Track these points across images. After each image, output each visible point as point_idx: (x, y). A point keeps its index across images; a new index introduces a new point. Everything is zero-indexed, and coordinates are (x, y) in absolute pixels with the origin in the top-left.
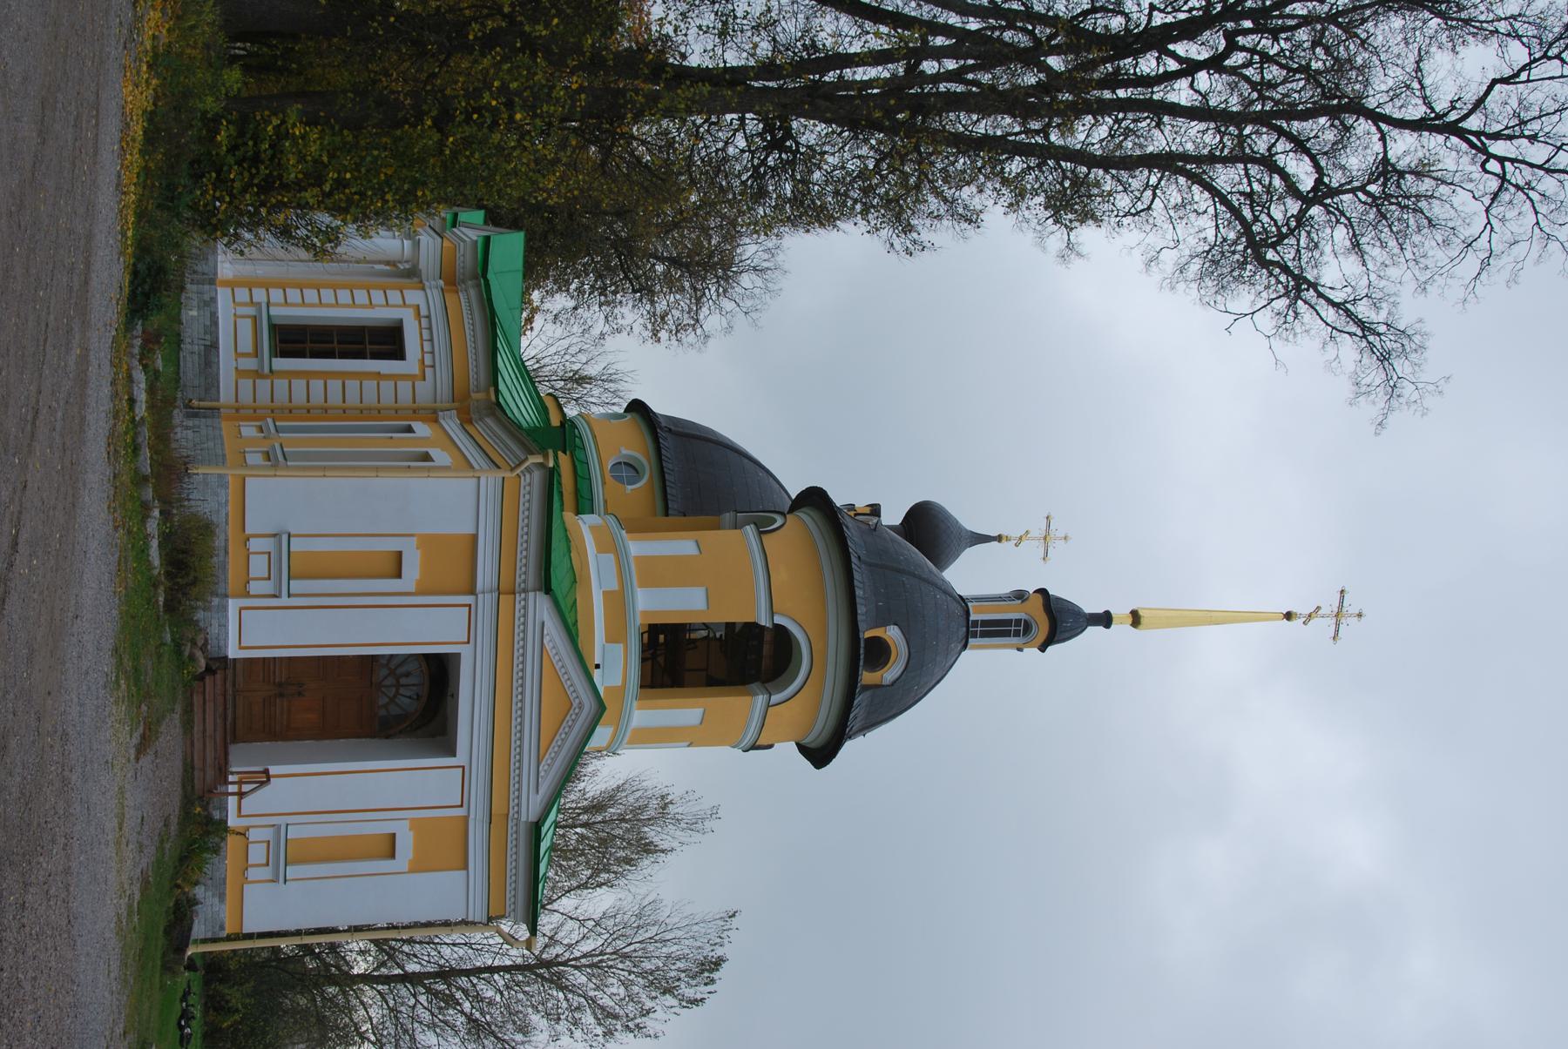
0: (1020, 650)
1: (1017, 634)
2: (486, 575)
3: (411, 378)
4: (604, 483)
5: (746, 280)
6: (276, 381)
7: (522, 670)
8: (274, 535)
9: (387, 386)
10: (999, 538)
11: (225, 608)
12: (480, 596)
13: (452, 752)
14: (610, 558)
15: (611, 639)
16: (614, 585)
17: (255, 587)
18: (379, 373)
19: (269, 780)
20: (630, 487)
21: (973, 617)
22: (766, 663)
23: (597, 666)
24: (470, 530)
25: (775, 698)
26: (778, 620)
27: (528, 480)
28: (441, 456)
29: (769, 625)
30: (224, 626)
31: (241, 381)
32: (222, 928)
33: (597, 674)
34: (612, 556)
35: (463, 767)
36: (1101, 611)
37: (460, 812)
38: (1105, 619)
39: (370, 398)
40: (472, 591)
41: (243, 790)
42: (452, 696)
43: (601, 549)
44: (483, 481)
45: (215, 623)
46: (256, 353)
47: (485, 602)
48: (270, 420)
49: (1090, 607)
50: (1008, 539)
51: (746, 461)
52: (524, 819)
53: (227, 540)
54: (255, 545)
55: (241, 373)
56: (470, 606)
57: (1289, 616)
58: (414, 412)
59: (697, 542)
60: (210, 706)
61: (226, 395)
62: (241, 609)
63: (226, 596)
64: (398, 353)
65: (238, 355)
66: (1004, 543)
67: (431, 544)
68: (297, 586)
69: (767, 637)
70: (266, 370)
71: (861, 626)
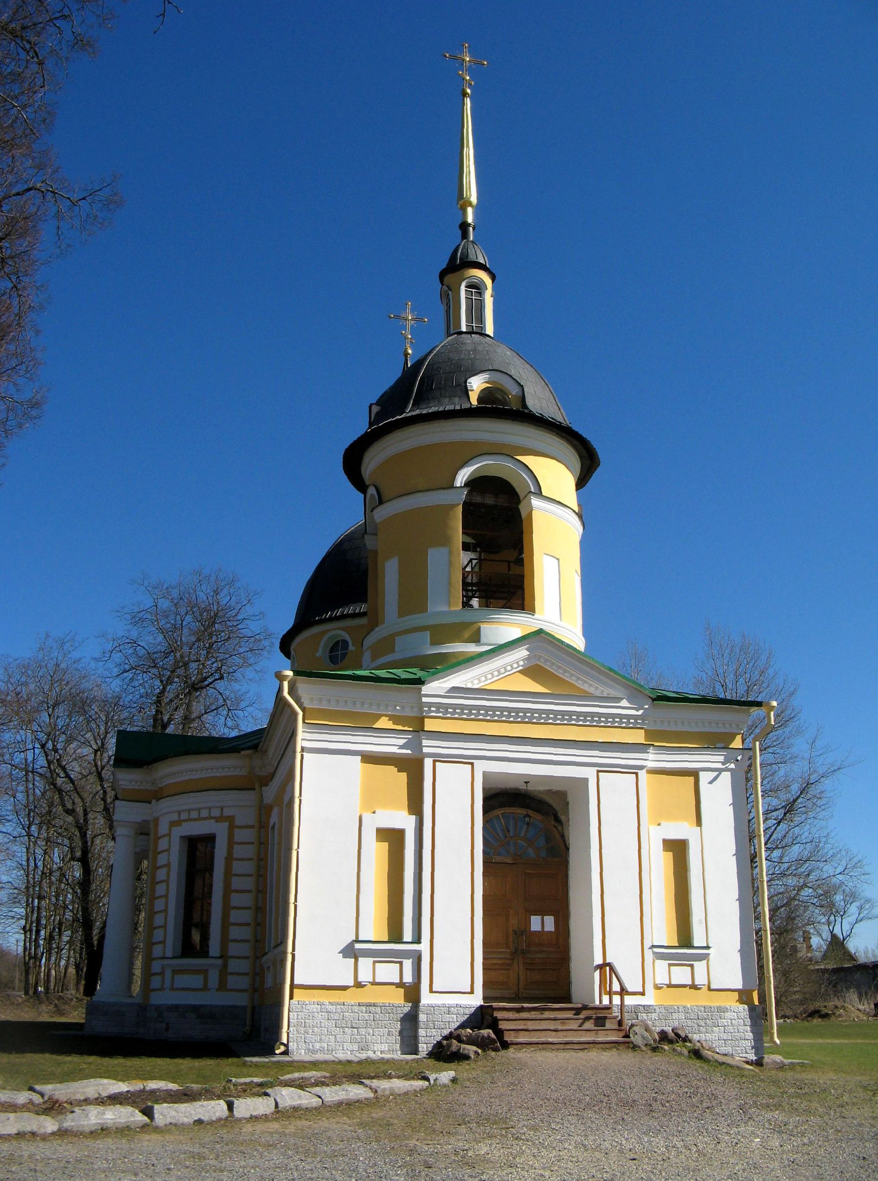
3: (232, 827)
5: (223, 598)
9: (238, 851)
19: (609, 965)
30: (449, 1009)
31: (229, 986)
34: (608, 996)
41: (619, 990)
42: (526, 783)
44: (307, 744)
45: (447, 1017)
46: (204, 972)
55: (222, 986)
56: (434, 761)
61: (242, 1000)
62: (431, 991)
64: (210, 839)
65: (205, 988)
67: (371, 801)
68: (408, 935)
69: (478, 499)
70: (219, 962)
71: (466, 406)
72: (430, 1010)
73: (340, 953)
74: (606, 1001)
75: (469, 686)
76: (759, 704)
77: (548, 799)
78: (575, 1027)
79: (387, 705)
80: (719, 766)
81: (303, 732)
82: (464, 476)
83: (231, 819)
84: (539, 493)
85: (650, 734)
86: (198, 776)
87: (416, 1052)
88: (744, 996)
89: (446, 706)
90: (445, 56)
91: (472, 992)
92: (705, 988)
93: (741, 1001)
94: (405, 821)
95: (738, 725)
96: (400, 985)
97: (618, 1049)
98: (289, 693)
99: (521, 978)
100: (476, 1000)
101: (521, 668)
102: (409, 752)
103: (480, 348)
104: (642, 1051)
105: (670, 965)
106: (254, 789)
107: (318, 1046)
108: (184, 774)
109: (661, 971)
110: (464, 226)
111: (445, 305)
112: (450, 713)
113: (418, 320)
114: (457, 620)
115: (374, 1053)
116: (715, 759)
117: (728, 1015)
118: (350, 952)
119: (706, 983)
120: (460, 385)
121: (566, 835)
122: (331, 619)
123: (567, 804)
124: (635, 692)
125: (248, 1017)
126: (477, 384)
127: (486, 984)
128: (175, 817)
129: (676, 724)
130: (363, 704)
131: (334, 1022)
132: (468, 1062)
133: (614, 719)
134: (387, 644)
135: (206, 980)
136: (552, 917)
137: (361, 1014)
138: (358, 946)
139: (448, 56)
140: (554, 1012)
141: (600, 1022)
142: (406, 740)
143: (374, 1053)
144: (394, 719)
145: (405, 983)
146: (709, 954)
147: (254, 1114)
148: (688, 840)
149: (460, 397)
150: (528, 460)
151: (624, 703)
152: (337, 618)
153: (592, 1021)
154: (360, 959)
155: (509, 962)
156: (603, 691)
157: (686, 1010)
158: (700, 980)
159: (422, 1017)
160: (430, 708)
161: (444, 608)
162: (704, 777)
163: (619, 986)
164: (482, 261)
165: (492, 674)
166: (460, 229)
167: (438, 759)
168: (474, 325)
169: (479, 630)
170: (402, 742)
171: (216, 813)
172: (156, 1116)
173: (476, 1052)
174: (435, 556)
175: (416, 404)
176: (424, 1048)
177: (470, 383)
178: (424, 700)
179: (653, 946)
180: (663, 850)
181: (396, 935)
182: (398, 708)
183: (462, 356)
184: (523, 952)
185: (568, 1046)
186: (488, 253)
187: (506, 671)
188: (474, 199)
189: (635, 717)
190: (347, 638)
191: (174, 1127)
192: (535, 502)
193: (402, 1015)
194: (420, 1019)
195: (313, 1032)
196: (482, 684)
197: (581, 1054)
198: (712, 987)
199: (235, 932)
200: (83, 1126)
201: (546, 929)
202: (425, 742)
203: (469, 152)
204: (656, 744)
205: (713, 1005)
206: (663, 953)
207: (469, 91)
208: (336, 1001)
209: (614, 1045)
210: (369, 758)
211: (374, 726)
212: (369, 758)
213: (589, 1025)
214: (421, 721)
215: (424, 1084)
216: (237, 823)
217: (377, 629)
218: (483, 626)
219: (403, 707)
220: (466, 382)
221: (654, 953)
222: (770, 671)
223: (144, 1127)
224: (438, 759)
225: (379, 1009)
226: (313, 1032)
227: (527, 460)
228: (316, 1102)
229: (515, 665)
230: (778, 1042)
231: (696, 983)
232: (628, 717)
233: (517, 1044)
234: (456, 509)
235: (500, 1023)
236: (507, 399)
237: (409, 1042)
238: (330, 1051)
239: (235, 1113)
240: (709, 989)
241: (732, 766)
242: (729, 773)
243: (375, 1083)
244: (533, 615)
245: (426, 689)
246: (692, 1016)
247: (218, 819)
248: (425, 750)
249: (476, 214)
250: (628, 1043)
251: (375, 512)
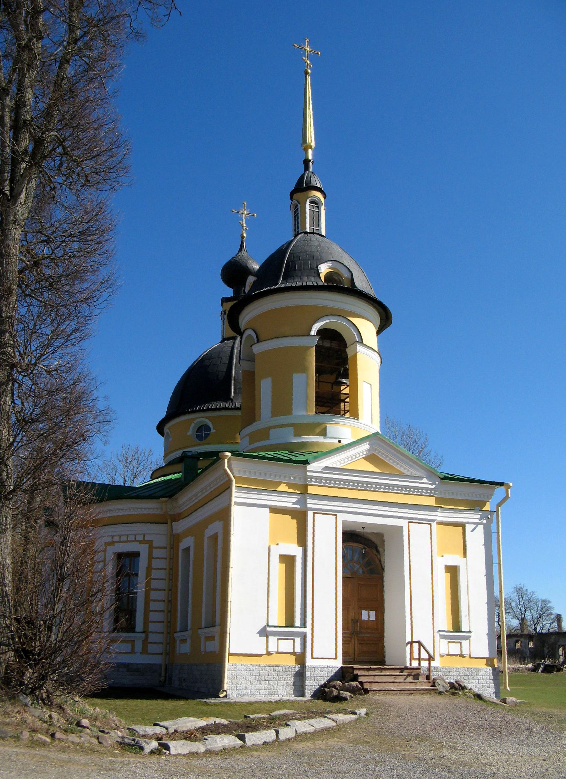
6: (150, 630)
9: (155, 564)
18: (147, 568)
20: (213, 431)
22: (335, 345)
23: (340, 441)
26: (314, 331)
30: (323, 669)
33: (344, 442)
35: (409, 522)
39: (162, 574)
42: (363, 528)
45: (322, 674)
48: (176, 635)
55: (144, 651)
56: (314, 513)
58: (172, 548)
60: (377, 679)
61: (157, 660)
62: (313, 658)
65: (133, 652)
67: (275, 537)
68: (298, 623)
70: (143, 635)
72: (312, 669)
73: (258, 633)
74: (415, 664)
75: (335, 466)
76: (501, 484)
77: (373, 539)
78: (402, 680)
79: (285, 477)
80: (477, 521)
81: (235, 492)
82: (316, 328)
83: (150, 542)
84: (361, 342)
85: (438, 500)
86: (119, 514)
87: (303, 695)
88: (489, 662)
89: (321, 479)
90: (294, 46)
91: (336, 658)
92: (468, 657)
93: (488, 665)
94: (296, 550)
95: (488, 496)
96: (293, 653)
97: (430, 694)
98: (228, 467)
99: (356, 649)
100: (338, 663)
101: (364, 456)
102: (298, 507)
103: (322, 244)
104: (445, 695)
106: (167, 523)
107: (244, 692)
108: (117, 511)
109: (443, 647)
110: (306, 162)
111: (294, 213)
112: (323, 483)
113: (251, 214)
114: (311, 421)
115: (278, 696)
116: (474, 517)
117: (481, 673)
118: (264, 632)
119: (469, 654)
120: (313, 269)
121: (382, 560)
122: (200, 411)
123: (384, 541)
124: (431, 474)
125: (163, 670)
126: (324, 269)
127: (345, 653)
128: (109, 540)
129: (445, 494)
130: (271, 475)
131: (254, 677)
132: (347, 702)
133: (418, 490)
134: (264, 433)
135: (133, 647)
136: (374, 612)
137: (270, 672)
138: (269, 629)
139: (296, 45)
140: (387, 671)
141: (416, 677)
142: (297, 499)
143: (278, 696)
144: (289, 485)
145: (296, 653)
146: (470, 636)
147: (287, 737)
148: (459, 566)
149: (314, 277)
150: (356, 321)
151: (425, 480)
152: (203, 411)
153: (412, 677)
154: (270, 637)
155: (349, 639)
156: (412, 473)
157: (458, 670)
158: (465, 652)
159: (308, 674)
160: (311, 479)
161: (303, 413)
162: (469, 528)
163: (428, 655)
164: (318, 185)
165: (348, 459)
166: (304, 164)
167: (316, 512)
168: (314, 228)
169: (325, 429)
170: (294, 500)
171: (140, 538)
172: (247, 740)
173: (350, 696)
174: (297, 379)
175: (285, 278)
176: (309, 693)
177: (320, 268)
178: (309, 474)
179: (439, 631)
180: (445, 572)
181: (290, 622)
182: (292, 478)
183: (313, 250)
184: (358, 633)
185: (402, 692)
186: (322, 181)
187: (356, 458)
188: (313, 144)
189: (431, 489)
190: (211, 425)
191: (255, 747)
192: (359, 348)
193: (295, 673)
194: (306, 675)
195: (241, 683)
196: (342, 465)
197: (411, 697)
198: (472, 656)
199: (153, 616)
200: (216, 747)
201: (371, 619)
202: (309, 501)
203: (310, 113)
204: (443, 506)
205: (472, 667)
206: (444, 635)
207: (309, 71)
208: (256, 663)
209: (428, 691)
210: (275, 510)
211: (277, 490)
212: (275, 510)
213: (410, 679)
214: (306, 487)
215: (353, 717)
216: (154, 545)
217: (254, 424)
218: (329, 426)
219: (295, 478)
220: (317, 267)
221: (440, 635)
222: (426, 450)
223: (241, 747)
224: (316, 512)
225: (281, 669)
226: (241, 683)
227: (355, 320)
228: (312, 729)
229: (361, 454)
230: (508, 689)
231: (463, 654)
232: (427, 489)
233: (373, 691)
234: (311, 349)
235: (359, 677)
236: (341, 280)
237: (300, 690)
238: (252, 695)
239: (279, 737)
240: (471, 657)
241: (485, 521)
242: (482, 526)
243: (334, 716)
244: (358, 420)
245: (309, 467)
246: (461, 673)
247: (141, 542)
248: (309, 506)
249: (313, 155)
250: (436, 690)
251: (253, 347)
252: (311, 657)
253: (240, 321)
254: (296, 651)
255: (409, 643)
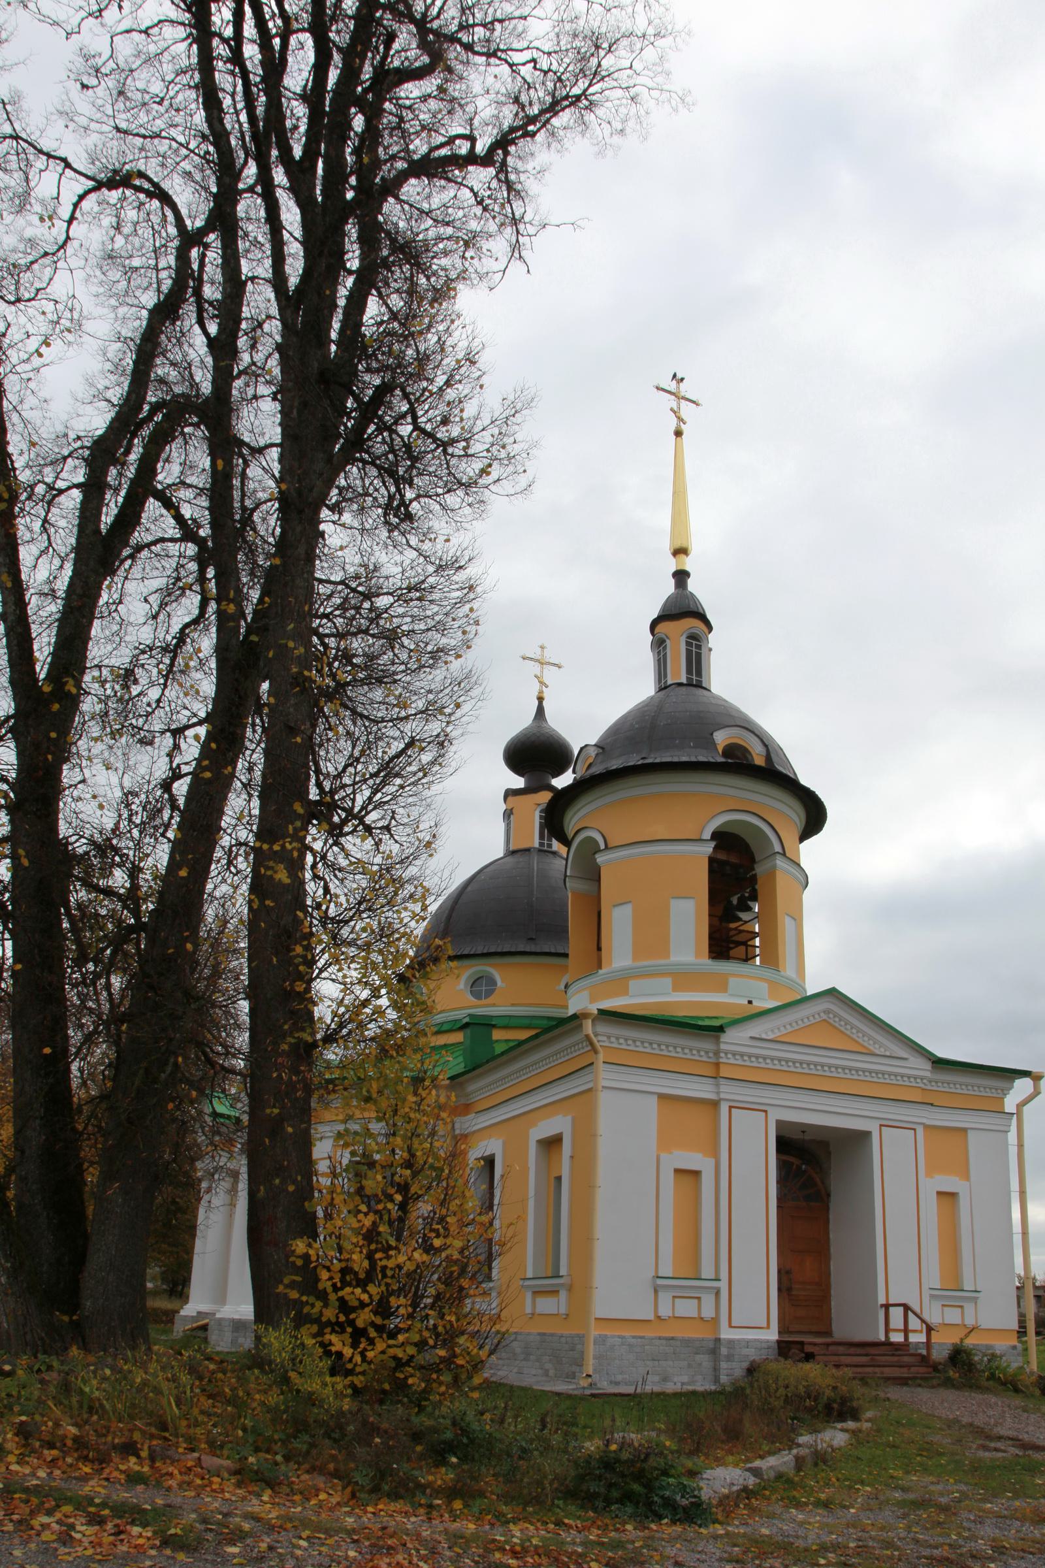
0: (710, 650)
1: (699, 647)
2: (702, 1090)
4: (494, 1005)
7: (794, 1063)
8: (656, 1292)
10: (540, 699)
11: (731, 1342)
12: (722, 1096)
13: (866, 1135)
14: (633, 984)
15: (723, 987)
16: (668, 982)
17: (708, 1312)
20: (499, 983)
21: (684, 681)
23: (750, 1002)
24: (653, 1101)
25: (778, 848)
26: (707, 835)
27: (605, 1038)
28: (557, 1124)
29: (713, 844)
30: (748, 1343)
32: (1014, 1347)
36: (672, 582)
37: (920, 1130)
38: (681, 576)
40: (715, 1104)
43: (625, 992)
45: (745, 1351)
47: (728, 1091)
49: (670, 587)
50: (541, 692)
51: (469, 888)
52: (928, 1074)
53: (660, 1338)
54: (665, 1311)
56: (731, 1107)
57: (678, 434)
59: (615, 906)
62: (730, 1326)
63: (718, 1340)
66: (545, 695)
67: (666, 1141)
68: (707, 1271)
91: (768, 1327)
105: (943, 1306)
212: (662, 1097)
225: (678, 1343)
252: (727, 1323)
253: (569, 815)
254: (966, 1323)
255: (882, 1306)
